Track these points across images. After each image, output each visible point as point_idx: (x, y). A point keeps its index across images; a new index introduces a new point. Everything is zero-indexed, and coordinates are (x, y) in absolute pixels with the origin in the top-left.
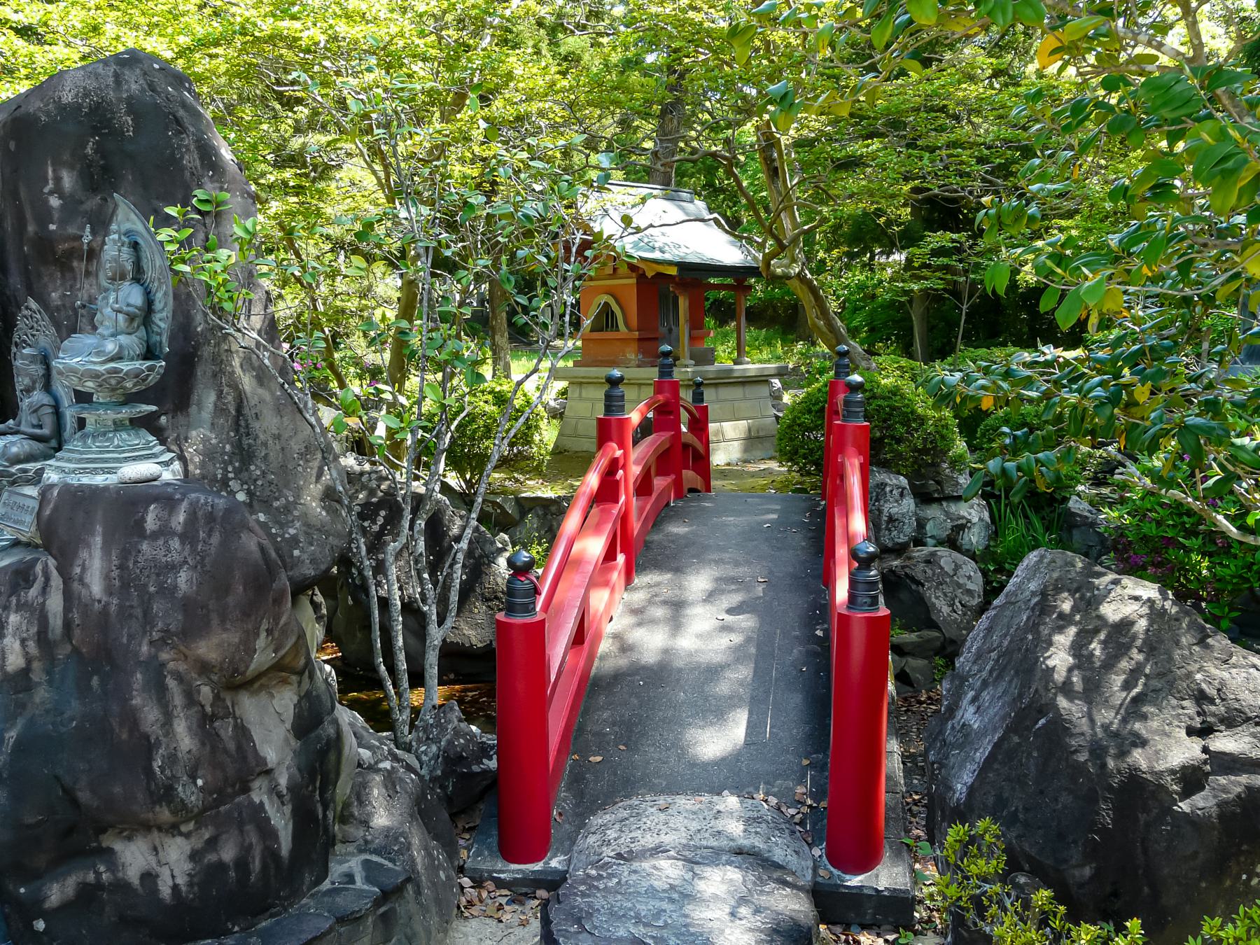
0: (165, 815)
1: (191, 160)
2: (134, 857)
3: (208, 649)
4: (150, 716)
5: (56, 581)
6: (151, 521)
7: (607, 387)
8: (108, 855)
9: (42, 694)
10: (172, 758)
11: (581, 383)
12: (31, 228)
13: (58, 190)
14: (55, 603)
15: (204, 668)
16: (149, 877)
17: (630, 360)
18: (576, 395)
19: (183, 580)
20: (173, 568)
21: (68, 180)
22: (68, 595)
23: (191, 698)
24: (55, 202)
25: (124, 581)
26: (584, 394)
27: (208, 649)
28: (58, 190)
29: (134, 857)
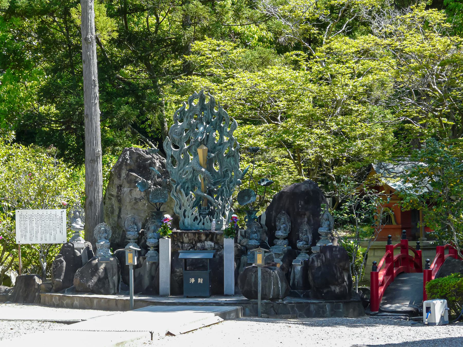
0: (337, 283)
1: (321, 199)
2: (333, 288)
3: (341, 264)
4: (335, 271)
5: (324, 256)
6: (334, 249)
7: (394, 83)
8: (330, 287)
9: (323, 269)
10: (337, 276)
11: (374, 249)
12: (296, 210)
13: (301, 204)
14: (324, 258)
15: (341, 266)
16: (334, 291)
17: (398, 238)
18: (372, 254)
19: (339, 256)
20: (338, 255)
21: (302, 203)
22: (325, 258)
23: (339, 270)
24: (300, 206)
25: (331, 256)
26: (376, 254)
27: (341, 264)
28: (301, 204)
29: (333, 288)
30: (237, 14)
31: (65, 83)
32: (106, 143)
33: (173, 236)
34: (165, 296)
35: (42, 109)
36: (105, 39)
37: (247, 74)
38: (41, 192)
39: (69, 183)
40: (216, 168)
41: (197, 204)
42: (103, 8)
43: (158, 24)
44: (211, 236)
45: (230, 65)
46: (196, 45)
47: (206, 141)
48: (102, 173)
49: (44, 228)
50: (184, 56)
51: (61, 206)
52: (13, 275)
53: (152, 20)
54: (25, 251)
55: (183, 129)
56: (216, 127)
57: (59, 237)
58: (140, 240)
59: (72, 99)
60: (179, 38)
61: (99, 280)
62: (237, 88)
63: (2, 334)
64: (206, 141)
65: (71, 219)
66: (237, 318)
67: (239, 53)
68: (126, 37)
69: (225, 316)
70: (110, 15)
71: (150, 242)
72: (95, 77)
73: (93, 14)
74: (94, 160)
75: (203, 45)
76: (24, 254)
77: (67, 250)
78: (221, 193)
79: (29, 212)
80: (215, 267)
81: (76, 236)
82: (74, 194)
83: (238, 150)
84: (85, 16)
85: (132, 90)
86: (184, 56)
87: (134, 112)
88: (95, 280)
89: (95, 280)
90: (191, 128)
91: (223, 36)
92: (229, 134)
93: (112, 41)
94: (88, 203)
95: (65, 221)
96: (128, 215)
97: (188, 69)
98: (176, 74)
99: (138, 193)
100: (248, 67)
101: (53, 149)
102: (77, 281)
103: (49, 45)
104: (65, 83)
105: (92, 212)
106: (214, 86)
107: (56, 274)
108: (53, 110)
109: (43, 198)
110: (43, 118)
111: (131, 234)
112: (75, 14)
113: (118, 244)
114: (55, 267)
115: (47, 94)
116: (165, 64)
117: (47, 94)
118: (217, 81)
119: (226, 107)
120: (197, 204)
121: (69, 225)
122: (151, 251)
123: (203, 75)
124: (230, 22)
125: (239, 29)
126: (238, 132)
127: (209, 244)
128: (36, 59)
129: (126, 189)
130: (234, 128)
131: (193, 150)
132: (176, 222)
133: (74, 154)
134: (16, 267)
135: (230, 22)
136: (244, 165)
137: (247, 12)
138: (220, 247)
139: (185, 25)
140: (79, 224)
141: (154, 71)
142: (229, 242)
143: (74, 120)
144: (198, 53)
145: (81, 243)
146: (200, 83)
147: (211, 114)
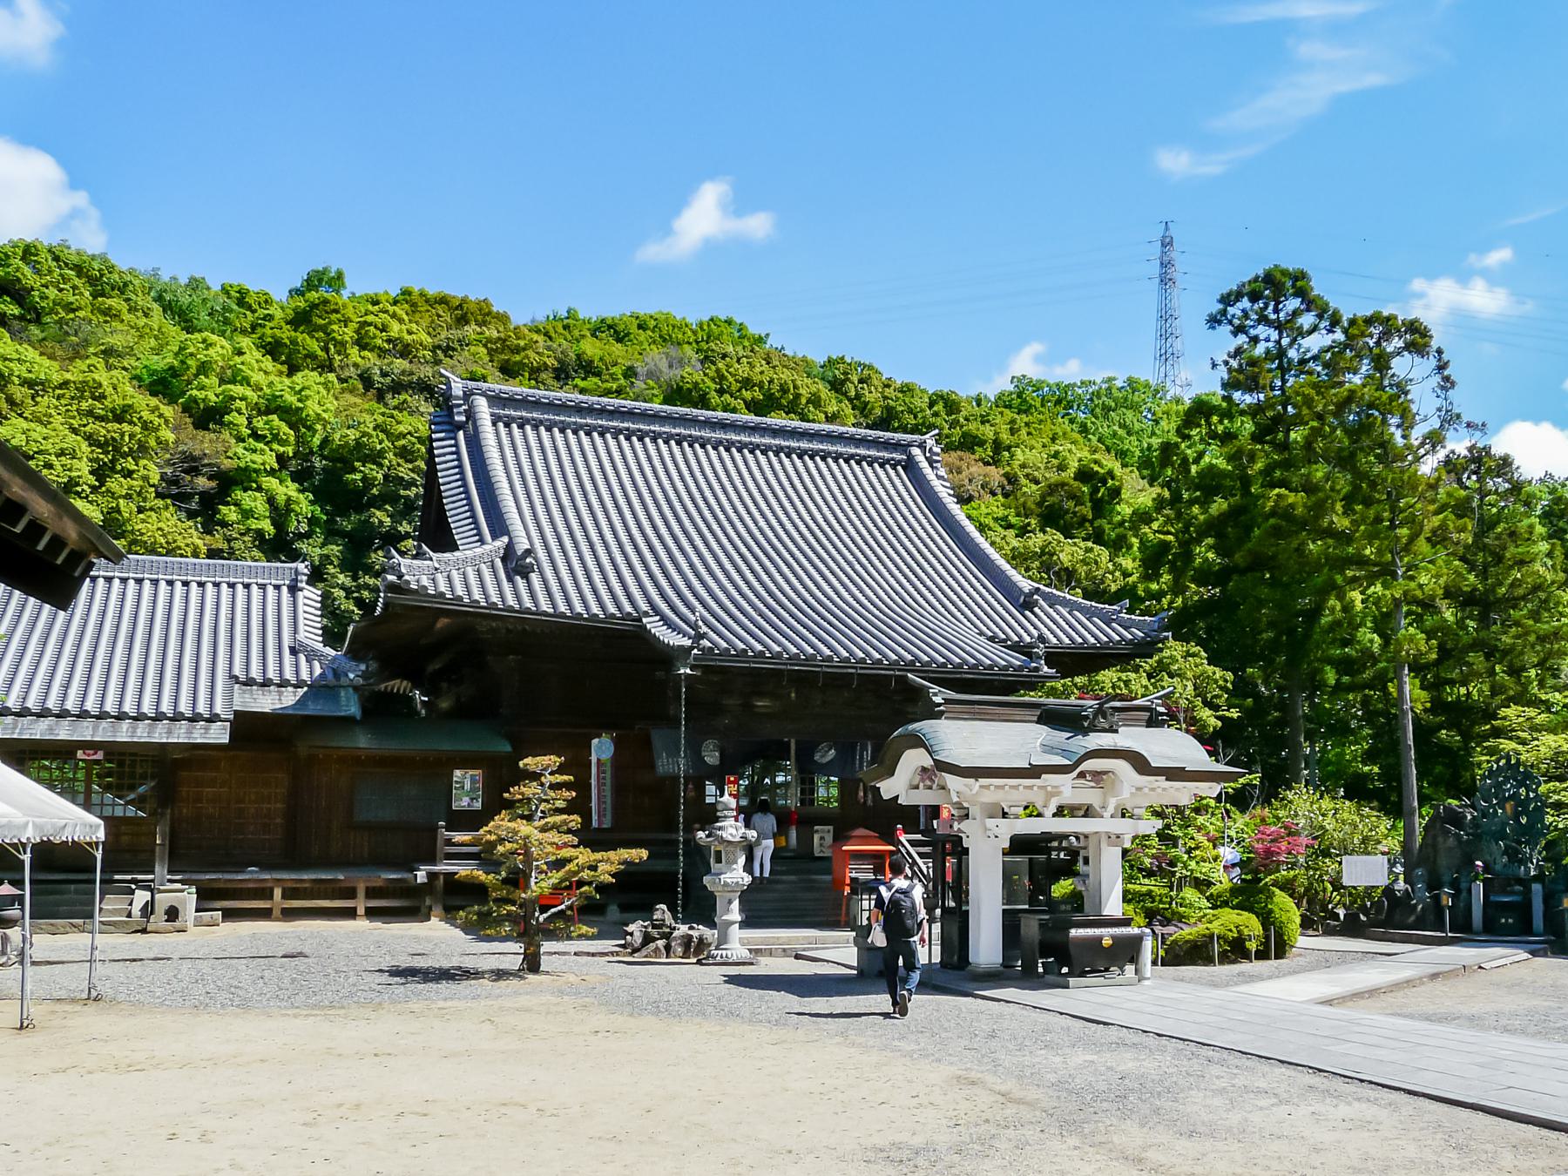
30: (1542, 685)
31: (1385, 748)
32: (1423, 799)
33: (1485, 881)
34: (1478, 934)
35: (1366, 769)
36: (1419, 708)
37: (1552, 737)
38: (1365, 840)
39: (1387, 834)
40: (1524, 821)
41: (1505, 852)
42: (1417, 681)
43: (1469, 694)
44: (1520, 881)
45: (1535, 728)
46: (1503, 712)
47: (1515, 796)
48: (1419, 824)
49: (1367, 872)
50: (131, 811)
51: (1383, 853)
52: (1341, 912)
53: (1463, 691)
54: (1352, 892)
55: (1491, 786)
56: (1521, 784)
57: (1382, 880)
58: (1454, 884)
59: (1391, 760)
60: (1488, 705)
61: (1418, 918)
62: (1542, 749)
63: (1256, 1170)
64: (1515, 796)
65: (1392, 864)
66: (1545, 955)
67: (1542, 718)
68: (1438, 706)
69: (1534, 953)
70: (1422, 688)
71: (1464, 885)
72: (1411, 742)
73: (1407, 688)
74: (1413, 814)
75: (1511, 712)
76: (1350, 894)
77: (1388, 891)
78: (1527, 843)
79: (1355, 858)
80: (1523, 911)
81: (1397, 879)
82: (1393, 844)
83: (1543, 804)
84: (1400, 690)
85: (1445, 750)
86: (131, 811)
87: (1447, 770)
88: (1412, 918)
89: (1412, 918)
90: (1498, 786)
91: (1529, 704)
92: (1535, 791)
93: (1425, 710)
94: (1406, 846)
95: (1386, 866)
96: (1443, 862)
97: (1497, 733)
98: (1486, 737)
99: (1451, 841)
100: (1553, 730)
101: (1375, 804)
102: (1397, 917)
103: (1370, 717)
104: (1385, 748)
105: (1410, 858)
106: (1520, 747)
107: (1379, 911)
108: (1376, 769)
109: (1366, 846)
110: (1367, 777)
111: (1446, 878)
112: (1392, 688)
113: (1434, 884)
114: (1377, 905)
115: (1369, 757)
116: (1477, 729)
117: (1369, 757)
118: (1524, 743)
119: (1532, 766)
120: (1505, 852)
121: (1391, 872)
122: (1464, 894)
123: (1510, 739)
124: (1535, 690)
125: (1544, 697)
126: (1543, 789)
127: (1518, 888)
128: (1361, 727)
129: (1440, 839)
130: (1539, 785)
131: (1501, 805)
132: (1486, 869)
133: (1394, 807)
134: (1344, 905)
135: (1535, 690)
136: (1549, 819)
137: (1550, 682)
138: (1528, 891)
139: (1494, 693)
140: (1399, 869)
141: (1467, 736)
142: (1537, 888)
143: (1393, 776)
144: (1504, 718)
145: (1401, 885)
146: (1507, 745)
147: (1521, 774)
